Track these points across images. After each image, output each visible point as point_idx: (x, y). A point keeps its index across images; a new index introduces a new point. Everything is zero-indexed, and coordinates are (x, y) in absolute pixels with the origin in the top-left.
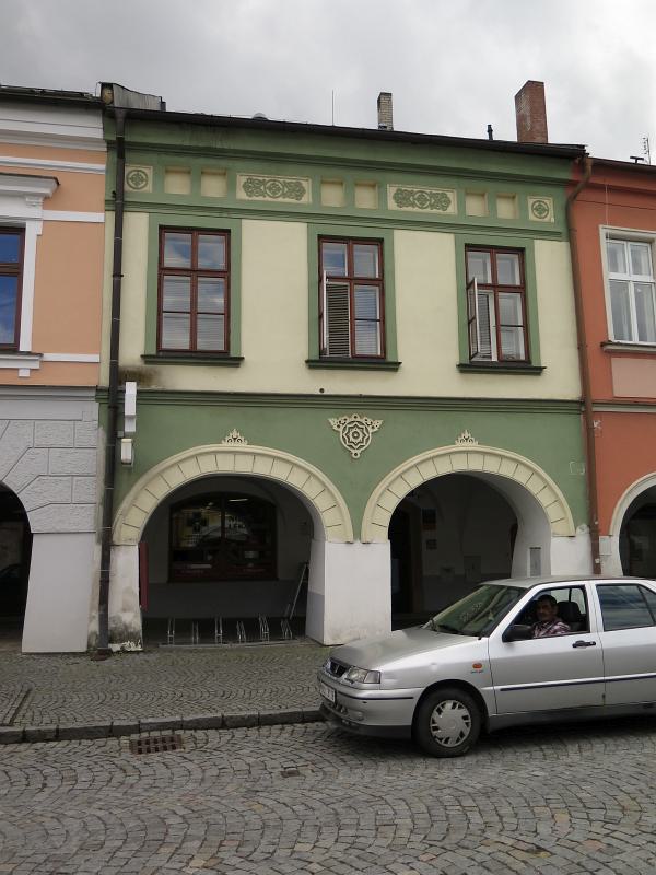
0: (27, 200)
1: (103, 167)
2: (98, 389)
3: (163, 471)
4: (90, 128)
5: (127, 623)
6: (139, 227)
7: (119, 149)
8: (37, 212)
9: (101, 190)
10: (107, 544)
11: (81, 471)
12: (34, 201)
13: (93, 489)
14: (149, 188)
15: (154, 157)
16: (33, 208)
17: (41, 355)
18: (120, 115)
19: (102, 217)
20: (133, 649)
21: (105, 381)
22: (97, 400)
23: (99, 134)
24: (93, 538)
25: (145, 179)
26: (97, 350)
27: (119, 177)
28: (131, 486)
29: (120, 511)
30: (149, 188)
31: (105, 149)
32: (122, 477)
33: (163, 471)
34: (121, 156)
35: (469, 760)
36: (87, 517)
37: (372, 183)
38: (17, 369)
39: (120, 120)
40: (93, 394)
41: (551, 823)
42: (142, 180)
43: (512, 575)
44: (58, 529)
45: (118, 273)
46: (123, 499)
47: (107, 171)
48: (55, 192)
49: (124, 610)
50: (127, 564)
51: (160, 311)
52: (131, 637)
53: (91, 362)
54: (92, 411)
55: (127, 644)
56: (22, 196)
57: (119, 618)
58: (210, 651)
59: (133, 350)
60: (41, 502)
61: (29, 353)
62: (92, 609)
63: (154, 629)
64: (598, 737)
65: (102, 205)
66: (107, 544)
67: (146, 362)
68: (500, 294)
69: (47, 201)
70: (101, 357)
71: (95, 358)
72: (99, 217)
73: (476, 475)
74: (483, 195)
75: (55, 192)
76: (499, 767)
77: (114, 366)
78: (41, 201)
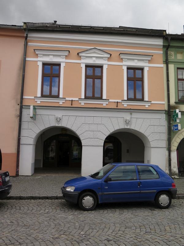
0: (104, 59)
1: (162, 52)
2: (165, 111)
3: (182, 132)
4: (159, 42)
5: (175, 171)
6: (172, 67)
7: (166, 48)
8: (147, 64)
9: (162, 58)
10: (169, 150)
11: (162, 132)
12: (63, 57)
13: (165, 137)
14: (173, 57)
15: (174, 49)
16: (106, 61)
17: (109, 100)
18: (169, 38)
19: (163, 66)
20: (177, 178)
21: (166, 108)
22: (165, 113)
23: (162, 44)
24: (165, 149)
25: (174, 55)
26: (164, 101)
27: (166, 55)
28: (174, 136)
29: (172, 142)
30: (173, 57)
31: (162, 47)
32: (172, 133)
33: (182, 132)
34: (167, 49)
35: (93, 212)
36: (164, 144)
37: (181, 52)
38: (145, 105)
39: (169, 40)
40: (164, 112)
41: (70, 233)
42: (171, 55)
43: (122, 161)
44: (158, 146)
45: (168, 80)
46: (173, 139)
47: (163, 53)
48: (151, 58)
49: (174, 168)
50: (174, 155)
51: (178, 90)
52: (176, 174)
53: (163, 104)
54: (163, 117)
55: (175, 176)
56: (60, 56)
57: (173, 170)
58: (134, 179)
59: (173, 101)
60: (153, 139)
61: (105, 100)
62: (166, 167)
63: (37, 170)
64: (109, 208)
65: (162, 63)
66: (169, 150)
67: (176, 104)
68: (179, 81)
69: (67, 57)
70: (165, 102)
71: (163, 103)
72: (162, 65)
73: (115, 132)
74: (182, 53)
75: (69, 55)
76: (130, 214)
77: (169, 105)
78: (148, 61)
